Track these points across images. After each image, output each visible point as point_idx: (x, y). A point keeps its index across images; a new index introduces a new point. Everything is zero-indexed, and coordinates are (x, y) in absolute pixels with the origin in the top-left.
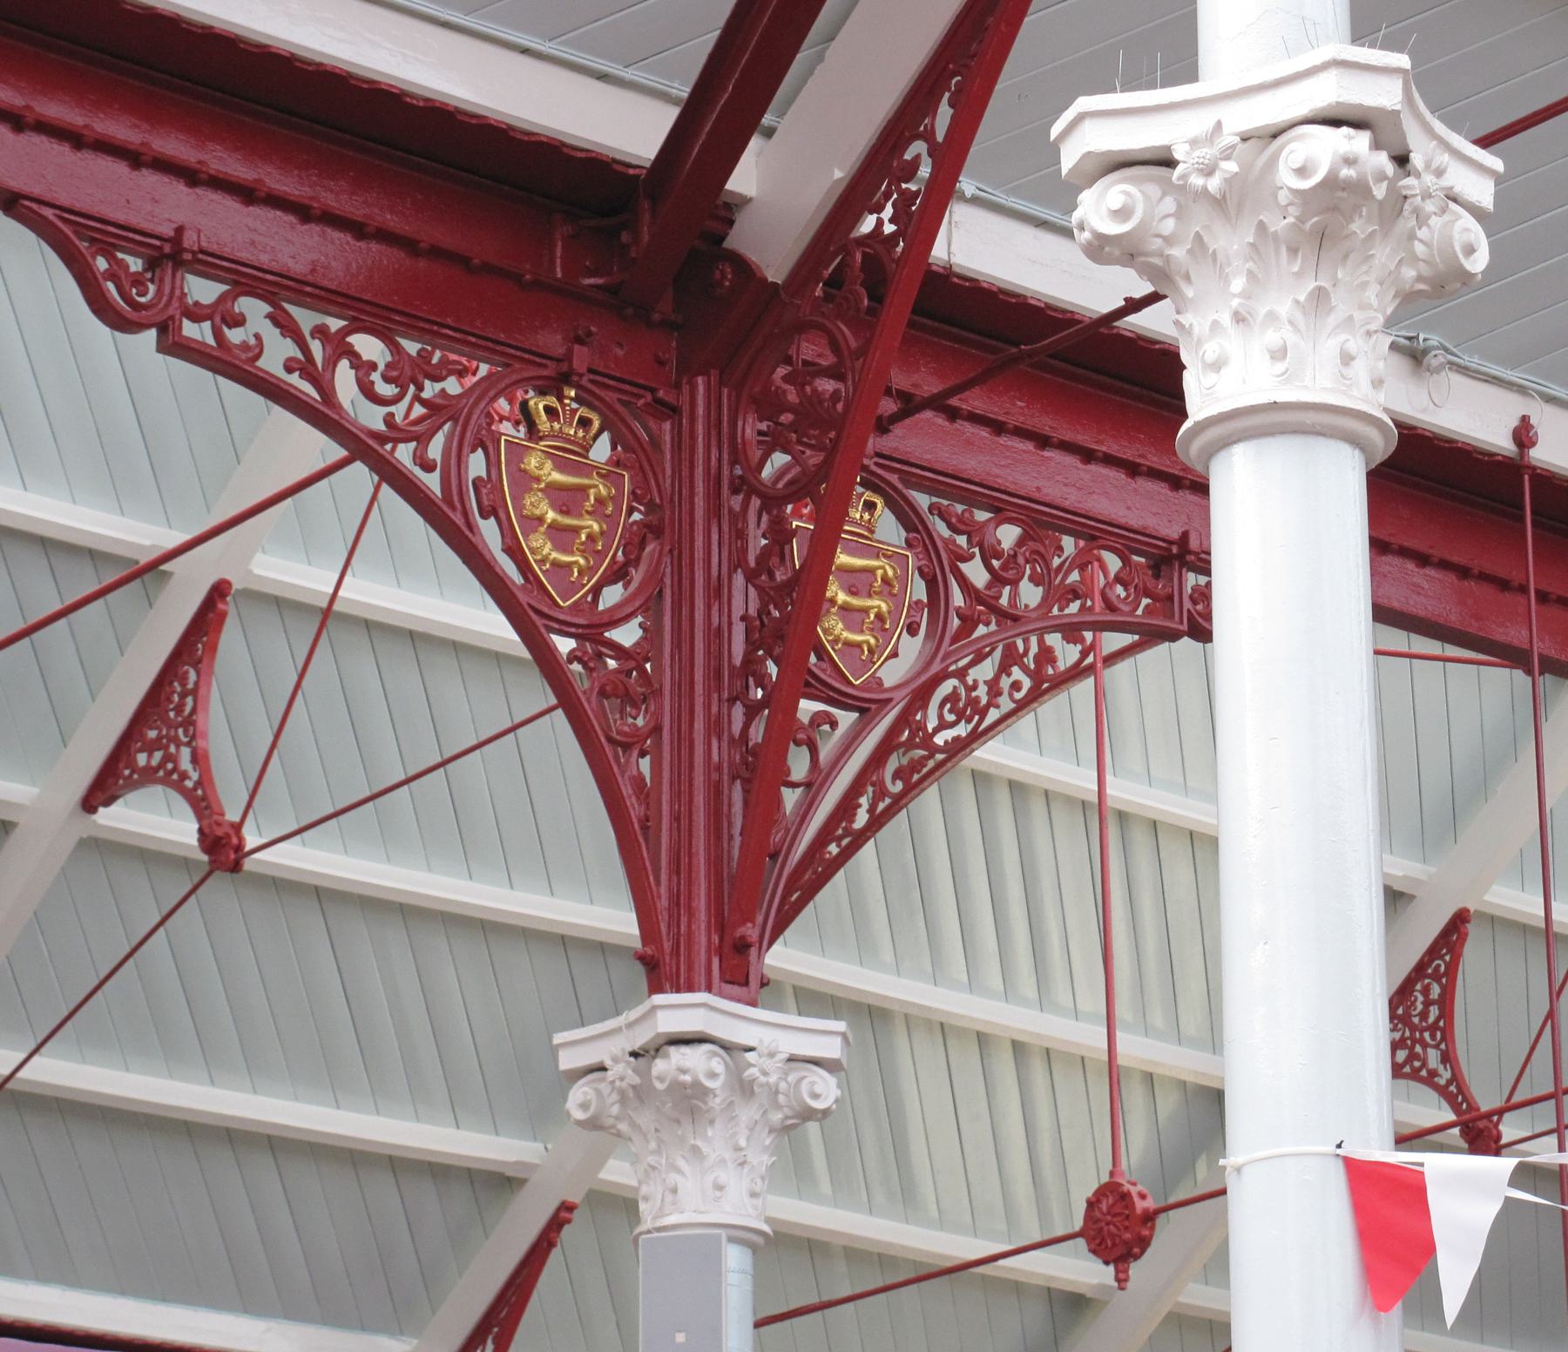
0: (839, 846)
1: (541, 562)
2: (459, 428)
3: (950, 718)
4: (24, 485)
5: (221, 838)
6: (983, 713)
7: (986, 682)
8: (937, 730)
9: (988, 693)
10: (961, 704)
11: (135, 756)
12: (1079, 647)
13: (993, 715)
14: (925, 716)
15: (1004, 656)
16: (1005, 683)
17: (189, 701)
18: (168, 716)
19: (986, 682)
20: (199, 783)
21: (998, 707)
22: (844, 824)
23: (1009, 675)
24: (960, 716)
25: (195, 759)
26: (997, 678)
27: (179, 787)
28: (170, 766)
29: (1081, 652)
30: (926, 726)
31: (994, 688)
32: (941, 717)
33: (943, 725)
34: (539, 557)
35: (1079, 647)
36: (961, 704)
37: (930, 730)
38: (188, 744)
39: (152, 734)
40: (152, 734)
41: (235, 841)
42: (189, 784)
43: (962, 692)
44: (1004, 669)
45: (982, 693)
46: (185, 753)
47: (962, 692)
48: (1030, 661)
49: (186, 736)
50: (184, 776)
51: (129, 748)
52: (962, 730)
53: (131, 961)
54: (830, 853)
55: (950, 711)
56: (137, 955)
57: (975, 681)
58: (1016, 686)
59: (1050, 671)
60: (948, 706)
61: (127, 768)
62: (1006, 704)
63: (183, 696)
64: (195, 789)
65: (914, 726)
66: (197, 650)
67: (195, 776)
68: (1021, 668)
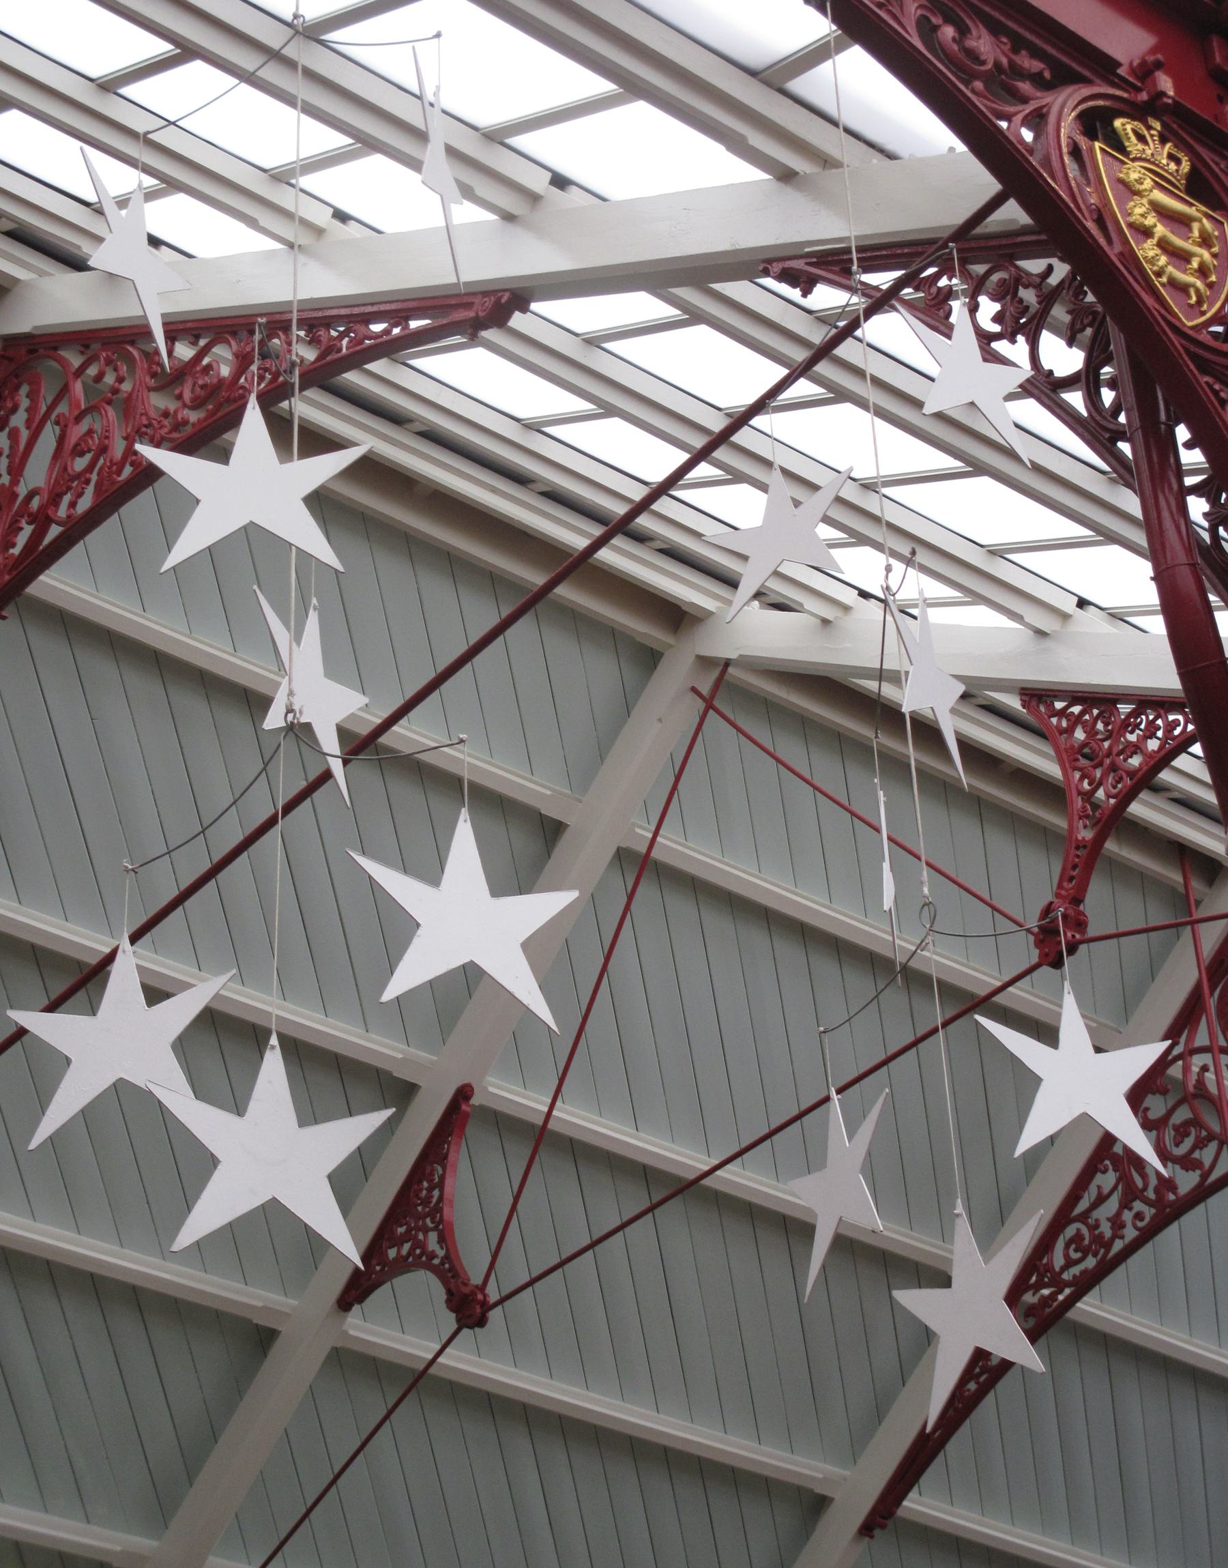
0: (977, 1383)
1: (1159, 274)
2: (1033, 238)
3: (1075, 1256)
4: (88, 1519)
5: (467, 1296)
6: (1108, 1245)
7: (1109, 1219)
8: (1065, 1268)
9: (1112, 1228)
10: (1086, 1242)
11: (386, 1251)
12: (1198, 1172)
13: (1118, 1245)
14: (1051, 1260)
15: (1125, 1194)
16: (1127, 1216)
17: (436, 1193)
18: (417, 1210)
19: (1109, 1219)
20: (447, 1257)
21: (1122, 1237)
22: (981, 1364)
23: (1130, 1209)
24: (1085, 1252)
25: (442, 1240)
26: (1119, 1214)
27: (429, 1267)
28: (418, 1251)
29: (1201, 1176)
30: (1053, 1266)
31: (1117, 1223)
32: (1066, 1256)
33: (1070, 1263)
34: (1155, 268)
35: (1198, 1172)
36: (1086, 1242)
37: (1057, 1269)
38: (435, 1229)
39: (401, 1230)
40: (401, 1230)
41: (480, 1297)
42: (436, 1261)
43: (1085, 1231)
44: (1125, 1205)
45: (1106, 1229)
46: (433, 1237)
47: (1085, 1231)
48: (1151, 1194)
49: (433, 1223)
50: (433, 1255)
51: (381, 1247)
52: (1090, 1262)
53: (360, 1457)
54: (969, 1390)
55: (1076, 1251)
56: (367, 1449)
57: (1097, 1220)
58: (1139, 1216)
59: (1172, 1197)
60: (1073, 1246)
61: (378, 1265)
62: (1130, 1233)
63: (430, 1190)
64: (442, 1263)
65: (1042, 1269)
66: (444, 1149)
67: (441, 1253)
68: (1142, 1201)
